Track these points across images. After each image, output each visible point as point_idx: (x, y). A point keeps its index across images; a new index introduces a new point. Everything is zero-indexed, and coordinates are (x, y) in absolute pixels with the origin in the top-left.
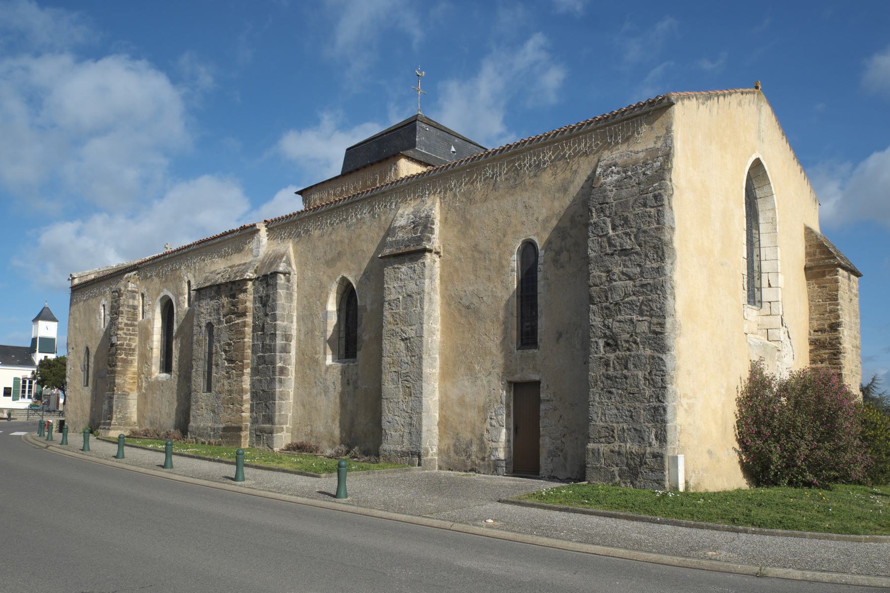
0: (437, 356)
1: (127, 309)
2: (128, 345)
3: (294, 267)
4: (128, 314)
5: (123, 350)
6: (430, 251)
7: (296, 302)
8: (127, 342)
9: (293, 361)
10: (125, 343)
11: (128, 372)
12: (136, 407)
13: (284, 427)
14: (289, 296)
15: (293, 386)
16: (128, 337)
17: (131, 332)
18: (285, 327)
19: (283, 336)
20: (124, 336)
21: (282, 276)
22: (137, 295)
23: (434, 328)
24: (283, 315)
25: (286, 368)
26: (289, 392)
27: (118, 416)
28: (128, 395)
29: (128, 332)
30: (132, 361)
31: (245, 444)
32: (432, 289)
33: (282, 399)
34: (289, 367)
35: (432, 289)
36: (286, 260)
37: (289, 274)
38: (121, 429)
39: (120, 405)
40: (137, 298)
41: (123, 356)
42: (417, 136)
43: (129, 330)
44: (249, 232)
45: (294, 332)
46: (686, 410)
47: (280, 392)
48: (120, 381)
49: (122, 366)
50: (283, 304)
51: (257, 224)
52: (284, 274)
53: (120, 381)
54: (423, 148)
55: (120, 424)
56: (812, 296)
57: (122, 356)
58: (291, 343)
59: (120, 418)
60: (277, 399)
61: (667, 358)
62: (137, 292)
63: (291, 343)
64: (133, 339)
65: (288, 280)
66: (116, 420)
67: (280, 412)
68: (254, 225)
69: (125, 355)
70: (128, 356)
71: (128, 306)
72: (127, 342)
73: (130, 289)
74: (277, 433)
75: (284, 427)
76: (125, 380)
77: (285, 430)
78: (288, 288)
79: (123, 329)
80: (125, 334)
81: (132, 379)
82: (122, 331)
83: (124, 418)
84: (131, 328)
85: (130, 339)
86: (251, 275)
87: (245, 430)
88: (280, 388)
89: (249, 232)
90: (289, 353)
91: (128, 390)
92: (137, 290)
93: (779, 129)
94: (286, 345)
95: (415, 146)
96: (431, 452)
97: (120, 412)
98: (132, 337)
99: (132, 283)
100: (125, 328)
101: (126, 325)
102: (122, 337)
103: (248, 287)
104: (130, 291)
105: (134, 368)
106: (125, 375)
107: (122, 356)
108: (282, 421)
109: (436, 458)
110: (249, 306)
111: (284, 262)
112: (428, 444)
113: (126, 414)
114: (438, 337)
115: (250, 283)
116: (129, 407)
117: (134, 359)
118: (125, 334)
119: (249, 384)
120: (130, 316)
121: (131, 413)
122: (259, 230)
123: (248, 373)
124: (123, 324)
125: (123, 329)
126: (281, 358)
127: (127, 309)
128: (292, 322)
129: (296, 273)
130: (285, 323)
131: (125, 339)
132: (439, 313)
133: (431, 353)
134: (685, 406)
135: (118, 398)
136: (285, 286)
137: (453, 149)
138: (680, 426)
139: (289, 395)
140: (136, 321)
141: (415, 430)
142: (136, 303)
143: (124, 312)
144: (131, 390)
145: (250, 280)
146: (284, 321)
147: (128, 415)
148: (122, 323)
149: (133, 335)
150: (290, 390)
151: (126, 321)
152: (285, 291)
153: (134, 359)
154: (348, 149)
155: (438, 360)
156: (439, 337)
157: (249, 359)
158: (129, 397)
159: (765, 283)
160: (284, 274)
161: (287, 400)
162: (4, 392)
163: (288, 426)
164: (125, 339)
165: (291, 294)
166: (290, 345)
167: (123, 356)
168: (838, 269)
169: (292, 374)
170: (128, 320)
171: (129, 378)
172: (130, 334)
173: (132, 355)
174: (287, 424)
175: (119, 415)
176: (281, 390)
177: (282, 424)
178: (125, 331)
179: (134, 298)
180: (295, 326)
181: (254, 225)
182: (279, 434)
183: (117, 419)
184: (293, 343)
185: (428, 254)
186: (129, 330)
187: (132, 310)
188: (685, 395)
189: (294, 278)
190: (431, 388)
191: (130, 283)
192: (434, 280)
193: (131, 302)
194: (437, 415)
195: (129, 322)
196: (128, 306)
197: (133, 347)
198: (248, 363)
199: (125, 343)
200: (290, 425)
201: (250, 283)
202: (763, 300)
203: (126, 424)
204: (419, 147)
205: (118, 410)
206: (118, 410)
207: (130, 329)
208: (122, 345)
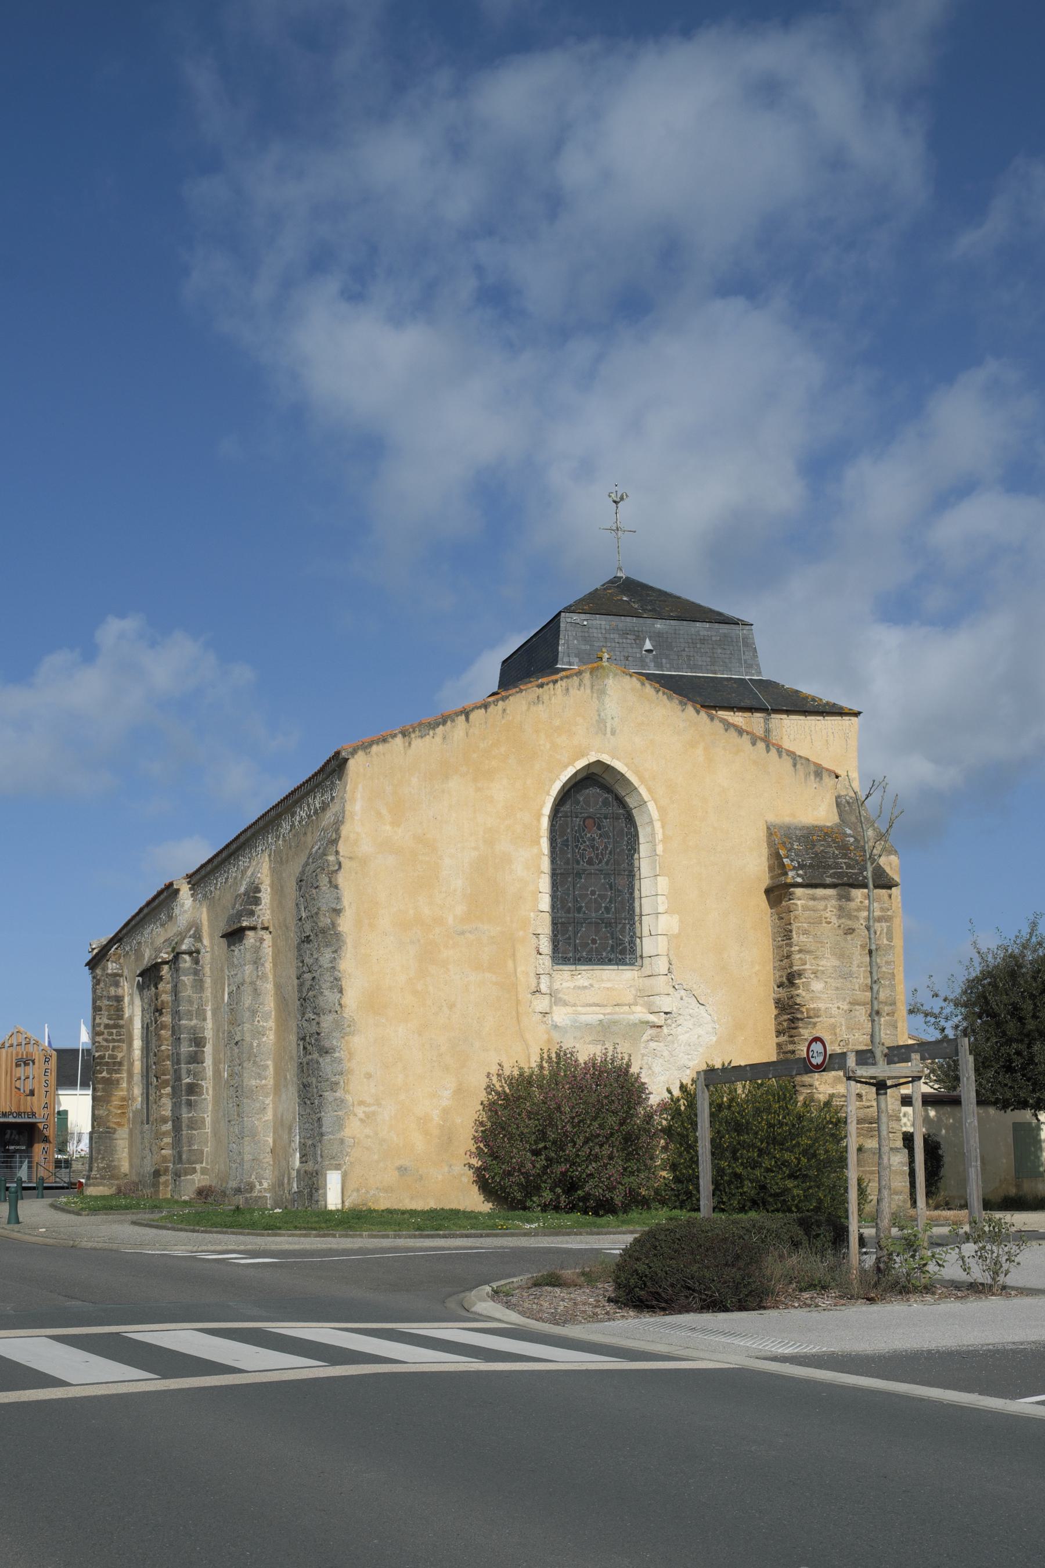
0: (270, 1063)
1: (108, 1003)
2: (112, 1057)
3: (206, 941)
4: (108, 1010)
5: (104, 1065)
6: (253, 928)
7: (210, 990)
8: (110, 1052)
9: (209, 1073)
10: (107, 1053)
11: (114, 1098)
12: (126, 1150)
13: (198, 1166)
14: (199, 985)
15: (210, 1108)
16: (111, 1045)
17: (115, 1037)
18: (194, 1028)
19: (191, 1040)
20: (105, 1044)
21: (187, 957)
22: (121, 979)
23: (263, 1027)
24: (189, 1011)
25: (197, 1085)
26: (204, 1118)
27: (101, 1165)
28: (114, 1133)
29: (110, 1038)
30: (118, 1081)
31: (165, 1194)
32: (258, 976)
33: (193, 1129)
34: (203, 1083)
35: (258, 976)
36: (194, 934)
37: (198, 952)
38: (104, 1185)
39: (102, 1148)
40: (122, 984)
41: (104, 1074)
42: (561, 642)
43: (111, 1034)
44: (169, 893)
45: (209, 1034)
46: (361, 1120)
47: (189, 1118)
48: (101, 1112)
49: (104, 1090)
50: (189, 996)
51: (174, 883)
52: (190, 953)
53: (101, 1112)
54: (576, 660)
55: (103, 1178)
56: (599, 960)
57: (103, 1075)
58: (205, 1049)
59: (104, 1168)
60: (184, 1128)
61: (325, 1061)
62: (121, 976)
63: (205, 1049)
64: (119, 1047)
65: (197, 962)
66: (98, 1171)
67: (190, 1146)
68: (171, 884)
69: (108, 1073)
70: (112, 1074)
71: (109, 998)
72: (110, 1052)
73: (109, 971)
74: (186, 1175)
75: (198, 1166)
76: (109, 1110)
77: (199, 1171)
78: (196, 973)
79: (102, 1034)
80: (106, 1040)
81: (119, 1108)
82: (101, 1037)
83: (110, 1167)
84: (114, 1031)
85: (114, 1047)
86: (165, 956)
87: (165, 1174)
88: (189, 1112)
89: (169, 893)
90: (203, 1063)
91: (114, 1126)
92: (120, 971)
93: (670, 698)
94: (196, 1052)
95: (556, 661)
96: (258, 1187)
97: (103, 1158)
98: (116, 1044)
99: (113, 962)
100: (106, 1031)
101: (107, 1026)
102: (102, 1046)
103: (163, 973)
104: (111, 975)
105: (122, 1091)
106: (108, 1102)
107: (103, 1075)
108: (193, 1158)
109: (268, 1195)
110: (165, 1000)
111: (190, 937)
112: (253, 1177)
113: (112, 1161)
114: (270, 1038)
115: (166, 967)
116: (116, 1151)
117: (123, 1078)
118: (106, 1040)
119: (170, 1108)
120: (112, 1013)
121: (119, 1160)
122: (177, 891)
123: (167, 1094)
124: (102, 1026)
125: (102, 1034)
126: (189, 1072)
127: (108, 1003)
128: (205, 1019)
129: (208, 949)
130: (194, 1022)
131: (107, 1048)
132: (272, 1005)
133: (258, 1059)
134: (361, 1115)
135: (99, 1138)
136: (192, 971)
137: (648, 645)
138: (353, 1138)
139: (203, 1122)
140: (122, 1019)
141: (963, 1182)
142: (120, 992)
143: (104, 1008)
144: (119, 1124)
145: (166, 963)
146: (191, 1020)
147: (116, 1163)
148: (100, 1024)
149: (119, 1041)
150: (206, 1116)
151: (106, 1021)
152: (191, 977)
153: (123, 1078)
154: (504, 662)
155: (271, 1068)
156: (272, 1037)
157: (169, 1074)
158: (116, 1136)
159: (646, 932)
160: (190, 953)
161: (200, 1129)
162: (913, 1140)
163: (204, 1165)
164: (107, 1048)
165: (201, 981)
166: (203, 1051)
167: (104, 1074)
168: (792, 889)
169: (208, 1094)
170: (110, 1019)
171: (115, 1108)
172: (114, 1041)
173: (118, 1072)
174: (202, 1163)
175: (102, 1163)
176: (191, 1115)
177: (193, 1163)
178: (106, 1036)
179: (117, 985)
180: (209, 1024)
181: (171, 884)
182: (189, 1177)
183: (99, 1169)
184: (208, 1049)
185: (250, 934)
186: (111, 1034)
187: (115, 1004)
188: (361, 1103)
189: (206, 958)
190: (258, 1105)
191: (109, 963)
192: (263, 965)
193: (112, 991)
194: (270, 1140)
195: (111, 1022)
196: (109, 998)
197: (118, 1060)
198: (167, 1081)
199: (107, 1053)
200: (207, 1163)
201: (166, 967)
202: (644, 955)
203: (112, 1177)
204: (566, 659)
205: (100, 1156)
206: (100, 1156)
207: (113, 1033)
208: (102, 1057)
